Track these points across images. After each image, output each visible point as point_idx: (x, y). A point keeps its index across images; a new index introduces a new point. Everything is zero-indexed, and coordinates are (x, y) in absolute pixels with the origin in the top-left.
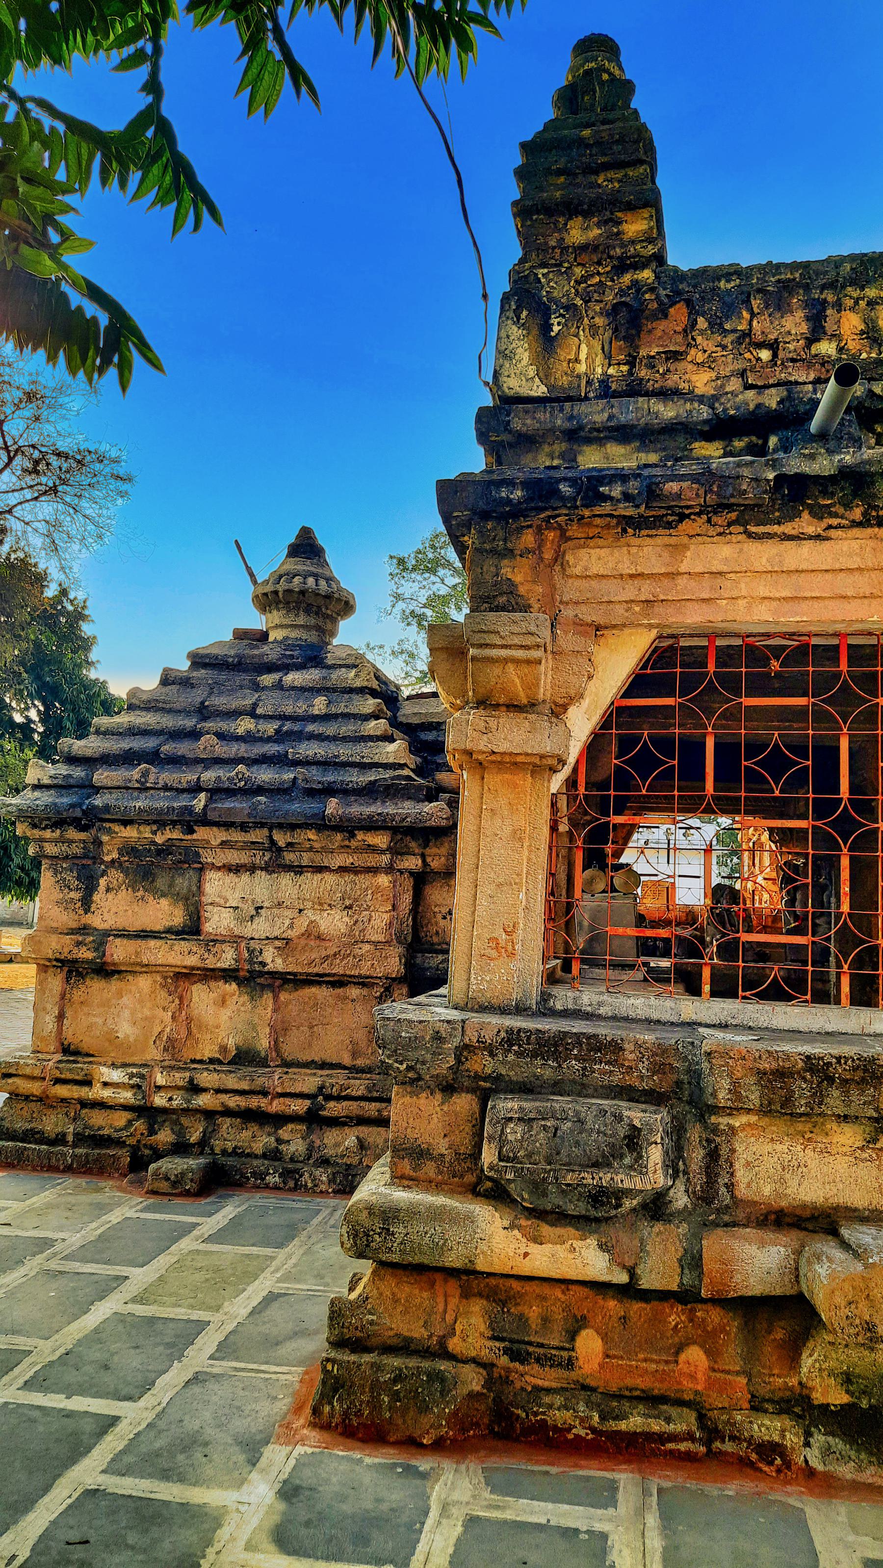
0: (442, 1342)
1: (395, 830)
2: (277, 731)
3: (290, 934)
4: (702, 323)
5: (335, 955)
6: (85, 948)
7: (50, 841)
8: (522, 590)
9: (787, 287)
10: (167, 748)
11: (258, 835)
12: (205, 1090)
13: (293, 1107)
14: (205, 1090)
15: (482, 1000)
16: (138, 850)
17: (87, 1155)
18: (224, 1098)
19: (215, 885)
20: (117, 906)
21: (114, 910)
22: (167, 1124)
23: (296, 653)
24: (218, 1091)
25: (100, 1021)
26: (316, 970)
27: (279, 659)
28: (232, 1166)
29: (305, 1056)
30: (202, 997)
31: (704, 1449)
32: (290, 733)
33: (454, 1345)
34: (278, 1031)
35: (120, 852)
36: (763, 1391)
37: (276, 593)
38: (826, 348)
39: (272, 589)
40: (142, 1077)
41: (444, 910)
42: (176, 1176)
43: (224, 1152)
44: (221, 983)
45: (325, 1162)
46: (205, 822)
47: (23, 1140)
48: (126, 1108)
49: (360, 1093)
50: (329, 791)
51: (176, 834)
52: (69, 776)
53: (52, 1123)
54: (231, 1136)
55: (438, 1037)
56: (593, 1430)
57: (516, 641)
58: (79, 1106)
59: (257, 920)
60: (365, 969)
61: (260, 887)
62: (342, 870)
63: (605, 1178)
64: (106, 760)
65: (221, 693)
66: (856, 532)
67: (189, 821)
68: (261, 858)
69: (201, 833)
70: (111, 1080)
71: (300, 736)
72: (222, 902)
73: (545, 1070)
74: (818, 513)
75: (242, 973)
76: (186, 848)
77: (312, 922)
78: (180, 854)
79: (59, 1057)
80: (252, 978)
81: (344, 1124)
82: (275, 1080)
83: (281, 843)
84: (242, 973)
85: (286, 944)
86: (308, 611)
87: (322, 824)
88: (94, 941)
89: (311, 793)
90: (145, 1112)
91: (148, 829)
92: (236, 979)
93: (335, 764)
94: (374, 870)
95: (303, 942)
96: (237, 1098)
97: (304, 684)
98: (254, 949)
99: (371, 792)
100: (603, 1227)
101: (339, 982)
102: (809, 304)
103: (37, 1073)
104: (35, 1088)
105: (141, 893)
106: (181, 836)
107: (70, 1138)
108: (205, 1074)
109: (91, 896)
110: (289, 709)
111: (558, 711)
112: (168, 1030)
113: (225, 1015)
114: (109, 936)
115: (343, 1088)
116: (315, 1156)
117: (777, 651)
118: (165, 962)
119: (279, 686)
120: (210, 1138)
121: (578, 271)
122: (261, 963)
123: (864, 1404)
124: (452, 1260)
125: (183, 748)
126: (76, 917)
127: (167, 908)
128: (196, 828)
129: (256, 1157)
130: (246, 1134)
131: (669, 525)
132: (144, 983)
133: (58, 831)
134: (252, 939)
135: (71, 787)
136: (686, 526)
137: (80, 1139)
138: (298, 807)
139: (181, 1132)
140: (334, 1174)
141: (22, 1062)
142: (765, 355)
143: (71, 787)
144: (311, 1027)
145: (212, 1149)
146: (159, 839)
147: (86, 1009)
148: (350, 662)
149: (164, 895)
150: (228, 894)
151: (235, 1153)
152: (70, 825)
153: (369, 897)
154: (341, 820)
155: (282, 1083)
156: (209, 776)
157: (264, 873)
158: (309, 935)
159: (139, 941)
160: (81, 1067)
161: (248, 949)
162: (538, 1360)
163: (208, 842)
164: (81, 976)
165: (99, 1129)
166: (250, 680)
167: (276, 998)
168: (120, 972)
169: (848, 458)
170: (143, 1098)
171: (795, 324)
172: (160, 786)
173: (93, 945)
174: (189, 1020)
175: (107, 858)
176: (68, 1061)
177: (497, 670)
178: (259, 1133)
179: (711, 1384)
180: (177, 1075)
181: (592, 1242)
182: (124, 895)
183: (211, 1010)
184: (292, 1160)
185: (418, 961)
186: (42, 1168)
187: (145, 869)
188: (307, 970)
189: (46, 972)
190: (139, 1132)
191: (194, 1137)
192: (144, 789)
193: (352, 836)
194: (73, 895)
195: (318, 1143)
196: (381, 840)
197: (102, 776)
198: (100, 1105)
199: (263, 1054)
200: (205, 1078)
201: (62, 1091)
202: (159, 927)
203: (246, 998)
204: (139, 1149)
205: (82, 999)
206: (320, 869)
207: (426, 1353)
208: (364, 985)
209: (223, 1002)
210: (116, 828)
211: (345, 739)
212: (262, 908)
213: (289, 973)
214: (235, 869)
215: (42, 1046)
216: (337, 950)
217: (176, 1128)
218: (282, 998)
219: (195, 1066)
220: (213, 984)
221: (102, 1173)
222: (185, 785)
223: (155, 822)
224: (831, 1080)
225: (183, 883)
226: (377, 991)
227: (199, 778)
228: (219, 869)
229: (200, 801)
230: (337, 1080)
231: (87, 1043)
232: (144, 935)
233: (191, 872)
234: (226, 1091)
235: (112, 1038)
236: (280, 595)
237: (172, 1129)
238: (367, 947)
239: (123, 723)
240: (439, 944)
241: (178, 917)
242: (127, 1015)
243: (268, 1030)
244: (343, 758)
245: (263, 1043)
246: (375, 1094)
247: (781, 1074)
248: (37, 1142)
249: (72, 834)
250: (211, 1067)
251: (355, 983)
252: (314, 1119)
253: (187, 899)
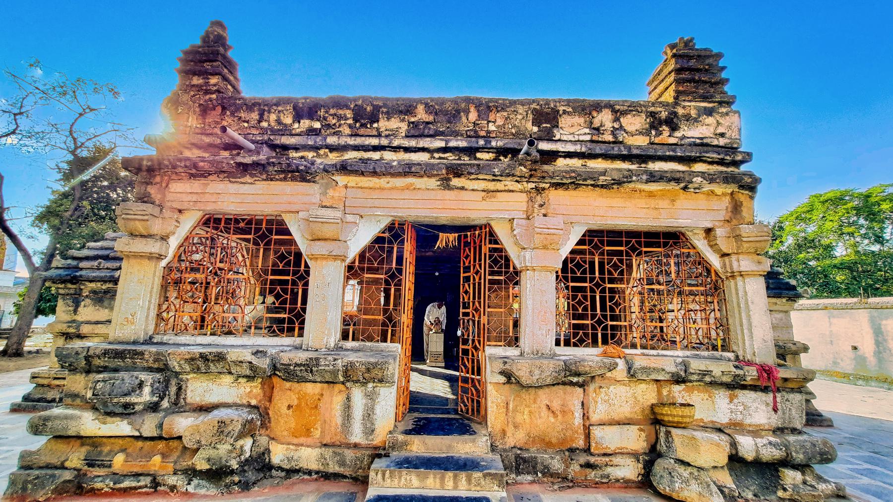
0: (63, 463)
4: (228, 113)
8: (153, 196)
9: (254, 105)
15: (119, 340)
31: (565, 482)
33: (67, 464)
35: (90, 292)
36: (178, 467)
38: (264, 124)
55: (77, 353)
56: (111, 488)
57: (139, 213)
63: (128, 399)
64: (87, 258)
66: (264, 182)
73: (119, 363)
74: (252, 176)
100: (132, 416)
102: (259, 110)
104: (45, 382)
111: (164, 238)
117: (243, 220)
121: (192, 93)
123: (214, 468)
124: (71, 433)
131: (205, 177)
136: (211, 177)
142: (246, 125)
146: (104, 287)
162: (98, 466)
164: (71, 338)
169: (255, 158)
171: (255, 116)
177: (132, 223)
179: (160, 467)
181: (125, 422)
197: (83, 264)
207: (56, 468)
224: (208, 360)
232: (97, 323)
247: (193, 359)
249: (69, 285)
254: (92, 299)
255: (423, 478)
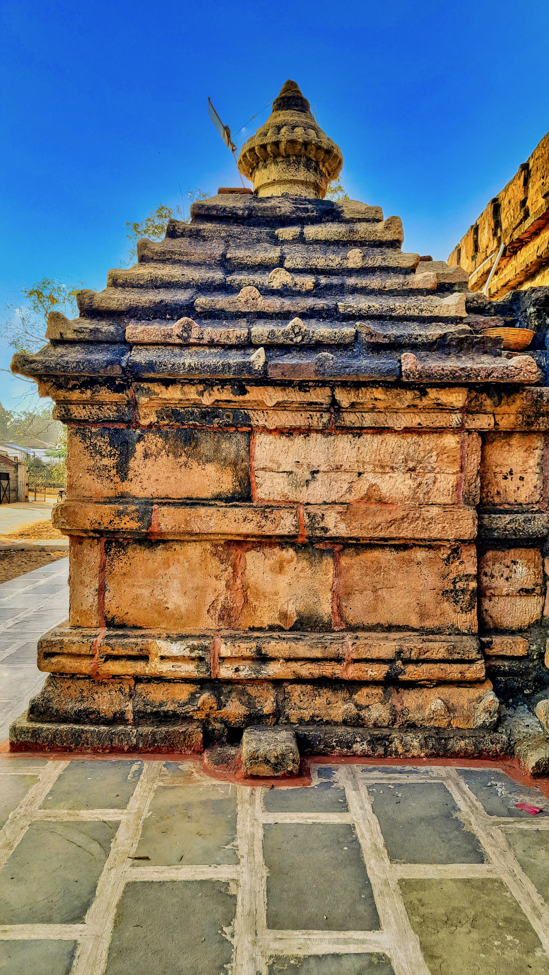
1: (470, 387)
2: (317, 285)
3: (349, 498)
5: (402, 519)
6: (127, 518)
7: (78, 403)
10: (202, 301)
11: (320, 396)
12: (273, 659)
13: (370, 673)
14: (273, 659)
16: (179, 414)
17: (154, 734)
18: (295, 666)
19: (265, 448)
20: (155, 472)
21: (154, 477)
22: (234, 694)
23: (310, 206)
24: (288, 660)
25: (146, 592)
26: (382, 534)
27: (293, 212)
28: (316, 737)
29: (371, 620)
30: (257, 566)
32: (329, 287)
34: (340, 597)
37: (277, 144)
39: (274, 139)
40: (205, 648)
41: (506, 470)
42: (277, 758)
43: (301, 721)
44: (277, 550)
45: (412, 726)
46: (264, 380)
47: (76, 722)
48: (186, 680)
49: (440, 656)
50: (396, 346)
51: (226, 395)
52: (97, 330)
53: (106, 701)
54: (305, 704)
58: (133, 682)
59: (312, 485)
60: (435, 532)
61: (316, 450)
62: (408, 430)
65: (238, 247)
67: (242, 381)
68: (320, 420)
69: (255, 394)
70: (170, 655)
71: (342, 290)
72: (275, 467)
75: (300, 540)
76: (234, 411)
77: (372, 485)
78: (228, 417)
79: (104, 632)
80: (312, 544)
81: (423, 686)
82: (347, 646)
83: (345, 404)
84: (300, 540)
85: (346, 509)
86: (308, 167)
87: (397, 382)
88: (137, 510)
89: (377, 348)
90: (210, 684)
91: (193, 389)
92: (293, 545)
93: (392, 318)
94: (439, 431)
95: (363, 506)
96: (309, 666)
97: (328, 237)
98: (315, 515)
99: (441, 346)
101: (403, 546)
103: (84, 650)
105: (183, 459)
106: (231, 397)
107: (130, 716)
108: (273, 643)
109: (127, 462)
110: (320, 262)
112: (222, 598)
113: (283, 581)
114: (152, 504)
115: (421, 651)
116: (400, 720)
118: (218, 530)
119: (301, 239)
120: (284, 707)
122: (323, 528)
125: (221, 301)
126: (112, 485)
127: (213, 473)
128: (248, 388)
129: (336, 724)
130: (320, 701)
132: (194, 551)
133: (89, 392)
134: (308, 504)
135: (100, 342)
137: (141, 717)
138: (367, 363)
139: (250, 703)
140: (425, 738)
141: (66, 639)
143: (100, 342)
144: (375, 590)
145: (287, 718)
146: (207, 400)
147: (130, 581)
148: (371, 216)
149: (209, 461)
150: (281, 459)
151: (313, 721)
152: (102, 385)
153: (434, 458)
154: (421, 376)
155: (357, 649)
156: (261, 330)
157: (319, 436)
158: (369, 499)
159: (188, 510)
160: (132, 643)
161: (309, 515)
163: (263, 403)
165: (161, 705)
166: (267, 234)
167: (336, 562)
168: (164, 542)
170: (208, 670)
172: (205, 341)
173: (136, 514)
174: (245, 588)
175: (144, 422)
176: (117, 636)
178: (333, 699)
180: (243, 645)
182: (165, 462)
183: (268, 577)
184: (375, 725)
185: (486, 521)
186: (104, 750)
187: (186, 431)
188: (372, 534)
189: (81, 543)
190: (207, 706)
191: (268, 707)
192: (185, 345)
193: (424, 394)
194: (106, 461)
195: (399, 707)
196: (456, 398)
197: (135, 330)
198: (160, 679)
199: (326, 619)
200: (273, 647)
201: (115, 667)
202: (207, 494)
203: (305, 563)
204: (209, 723)
205: (124, 570)
206: (379, 430)
208: (430, 547)
209: (280, 568)
210: (157, 388)
211: (392, 293)
212: (317, 472)
213: (351, 538)
214: (288, 432)
215: (82, 621)
216: (405, 513)
217: (245, 699)
218: (343, 563)
219: (256, 634)
220: (267, 550)
221: (173, 751)
222: (234, 341)
223: (201, 382)
225: (230, 447)
226: (444, 553)
227: (249, 333)
228: (270, 432)
229: (258, 358)
230: (413, 644)
231: (133, 615)
233: (239, 436)
234: (296, 660)
235: (161, 610)
236: (282, 146)
237: (240, 700)
238: (435, 511)
239: (143, 275)
240: (501, 505)
241: (227, 483)
242: (173, 588)
243: (330, 595)
244: (400, 312)
245: (325, 609)
246: (456, 657)
248: (92, 723)
249: (105, 395)
250: (275, 634)
251: (420, 546)
252: (392, 683)
253: (235, 465)
254: (166, 437)
255: (67, 348)
